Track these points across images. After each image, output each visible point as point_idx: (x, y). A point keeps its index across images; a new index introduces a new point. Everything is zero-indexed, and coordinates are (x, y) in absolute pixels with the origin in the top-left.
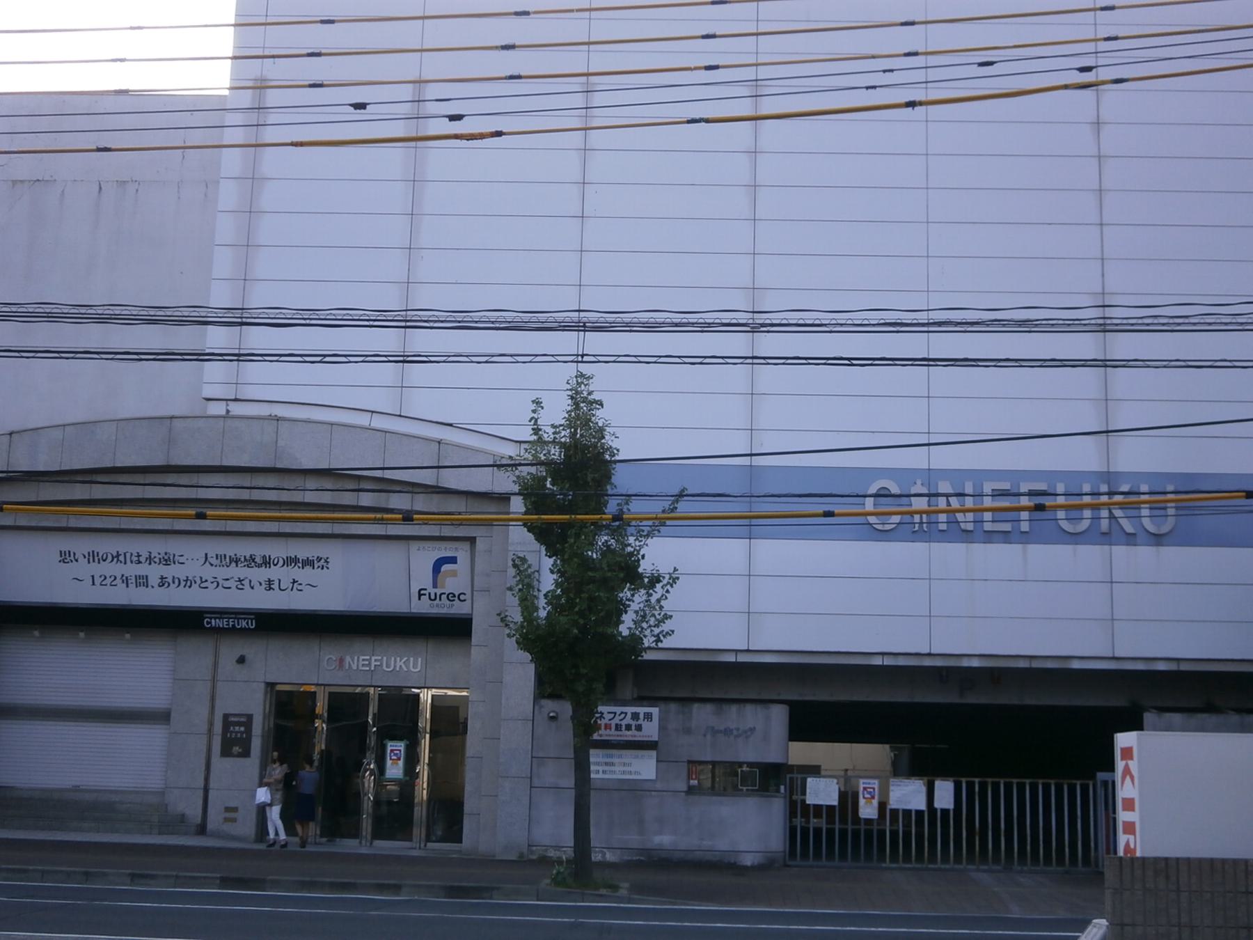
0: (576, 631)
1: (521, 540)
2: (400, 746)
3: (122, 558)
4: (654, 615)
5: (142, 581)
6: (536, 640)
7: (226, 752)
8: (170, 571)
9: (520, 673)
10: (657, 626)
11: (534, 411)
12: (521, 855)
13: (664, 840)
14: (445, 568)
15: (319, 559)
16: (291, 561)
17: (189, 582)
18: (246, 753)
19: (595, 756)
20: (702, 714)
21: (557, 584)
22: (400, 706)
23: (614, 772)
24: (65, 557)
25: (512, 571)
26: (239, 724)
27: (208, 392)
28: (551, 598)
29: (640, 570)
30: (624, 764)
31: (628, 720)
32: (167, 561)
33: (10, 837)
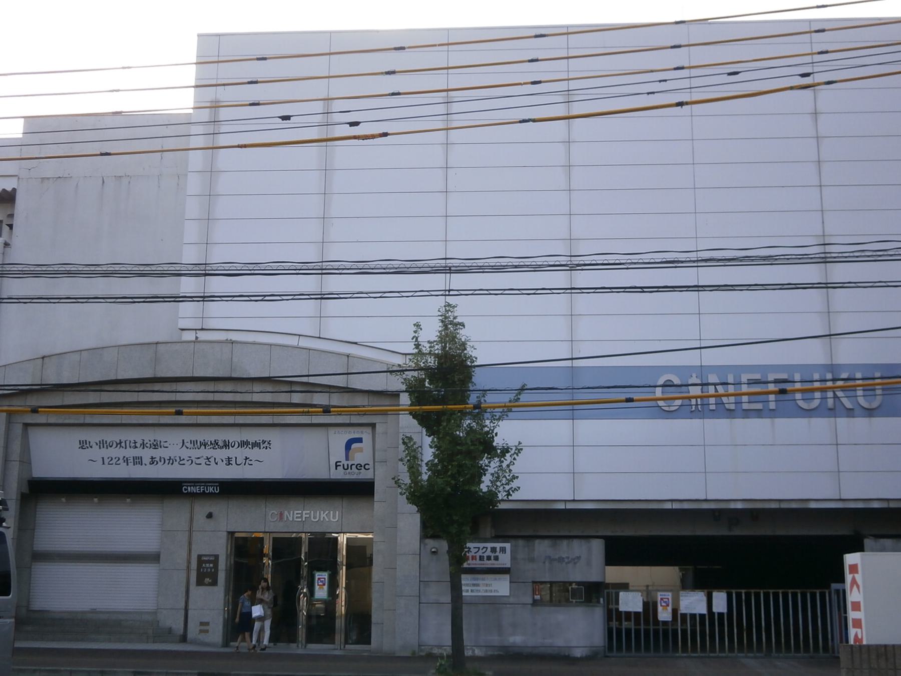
0: (449, 489)
1: (408, 425)
2: (325, 575)
3: (123, 444)
4: (505, 477)
5: (138, 461)
6: (421, 497)
7: (200, 583)
8: (158, 453)
9: (410, 520)
10: (507, 484)
11: (415, 332)
12: (414, 653)
13: (516, 639)
14: (354, 446)
15: (264, 442)
16: (244, 444)
18: (214, 583)
19: (466, 579)
20: (542, 548)
21: (435, 456)
24: (83, 445)
25: (402, 447)
26: (209, 562)
27: (181, 326)
28: (431, 466)
30: (487, 585)
31: (489, 553)
32: (155, 446)
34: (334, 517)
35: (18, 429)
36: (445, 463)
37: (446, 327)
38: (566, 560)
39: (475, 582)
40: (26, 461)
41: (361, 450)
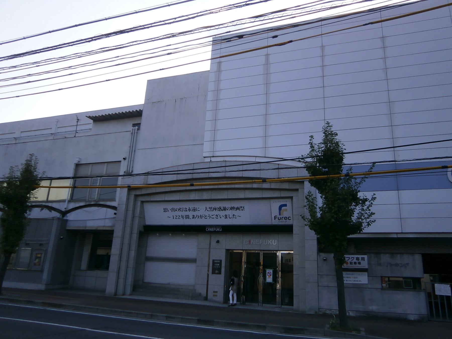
0: (333, 220)
1: (307, 186)
2: (271, 271)
3: (181, 210)
4: (366, 213)
5: (187, 217)
6: (316, 225)
7: (213, 273)
8: (196, 213)
9: (311, 238)
10: (368, 218)
11: (310, 140)
12: (316, 312)
13: (374, 308)
14: (283, 208)
15: (241, 207)
16: (232, 208)
17: (201, 217)
18: (220, 273)
19: (345, 274)
20: (385, 258)
21: (324, 204)
22: (270, 258)
23: (350, 281)
24: (165, 210)
25: (306, 200)
26: (217, 263)
27: (205, 155)
28: (321, 209)
29: (358, 197)
30: (355, 278)
31: (355, 260)
32: (194, 210)
33: (159, 300)
34: (274, 243)
35: (139, 204)
36: (330, 206)
37: (326, 136)
38: (400, 265)
39: (348, 276)
40: (142, 216)
41: (286, 210)
